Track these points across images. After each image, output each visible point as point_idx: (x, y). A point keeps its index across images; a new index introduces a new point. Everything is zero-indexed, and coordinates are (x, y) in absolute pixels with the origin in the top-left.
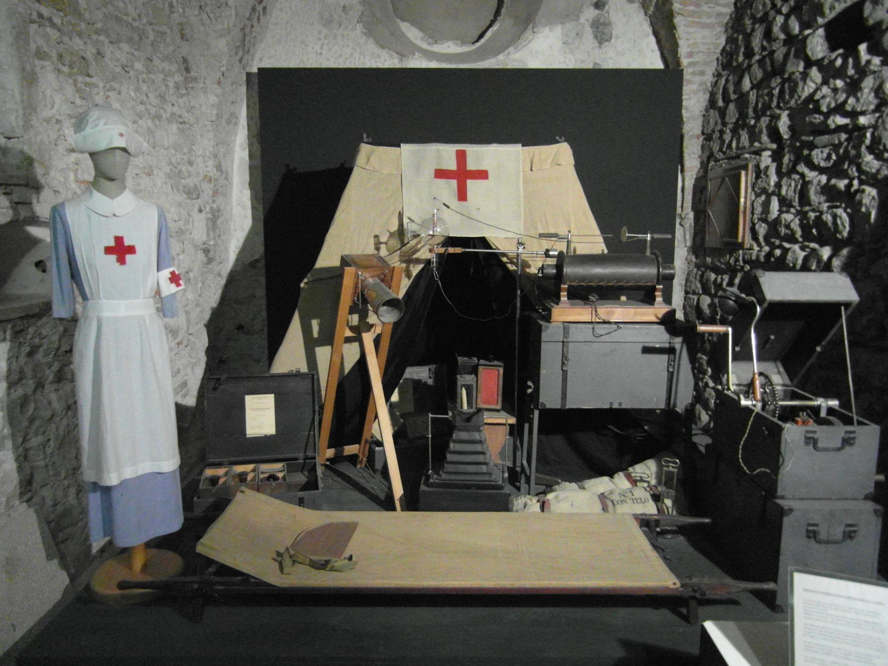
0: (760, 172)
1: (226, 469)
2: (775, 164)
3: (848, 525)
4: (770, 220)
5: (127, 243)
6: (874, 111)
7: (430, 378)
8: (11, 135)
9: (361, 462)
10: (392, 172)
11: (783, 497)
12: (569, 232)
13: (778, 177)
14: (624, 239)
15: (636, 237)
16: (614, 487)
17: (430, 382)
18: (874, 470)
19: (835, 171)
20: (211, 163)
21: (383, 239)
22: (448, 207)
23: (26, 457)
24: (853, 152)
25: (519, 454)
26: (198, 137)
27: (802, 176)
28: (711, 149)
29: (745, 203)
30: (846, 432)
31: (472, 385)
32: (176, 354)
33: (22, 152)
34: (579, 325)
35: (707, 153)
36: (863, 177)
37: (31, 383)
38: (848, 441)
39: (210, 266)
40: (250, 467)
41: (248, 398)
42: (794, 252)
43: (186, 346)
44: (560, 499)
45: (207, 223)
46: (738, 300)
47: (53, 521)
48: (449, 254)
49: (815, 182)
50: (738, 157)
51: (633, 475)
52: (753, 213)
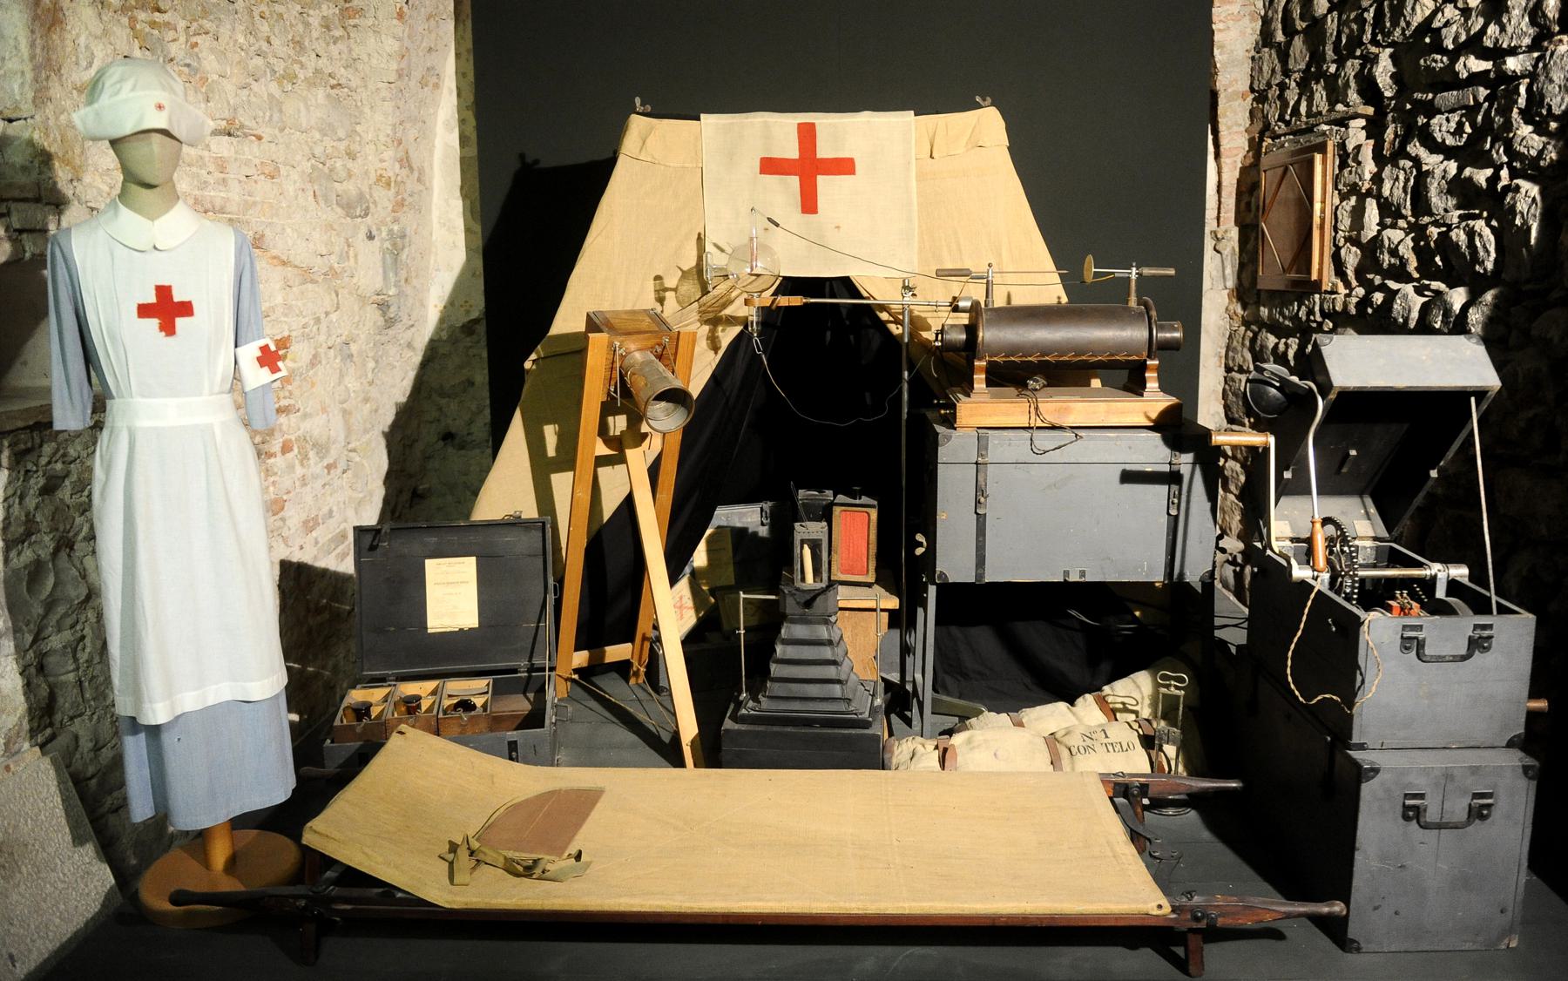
0: (1348, 155)
1: (386, 690)
2: (1372, 142)
3: (1476, 796)
4: (1364, 241)
5: (178, 297)
6: (1530, 49)
7: (763, 524)
8: (13, 116)
9: (637, 674)
10: (687, 165)
11: (1362, 747)
12: (990, 265)
13: (1376, 166)
14: (1089, 278)
15: (1113, 273)
16: (1076, 722)
17: (763, 532)
18: (1526, 693)
19: (1470, 154)
20: (389, 154)
21: (671, 282)
22: (777, 225)
23: (41, 668)
24: (1498, 120)
25: (909, 660)
26: (367, 110)
27: (1417, 162)
28: (1265, 117)
29: (1323, 211)
30: (1476, 627)
31: (821, 540)
32: (324, 485)
33: (30, 143)
34: (1005, 433)
35: (1259, 125)
36: (1517, 165)
37: (47, 542)
38: (1478, 644)
40: (431, 685)
41: (431, 565)
42: (1405, 296)
43: (344, 472)
44: (976, 744)
45: (384, 259)
46: (1284, 386)
48: (779, 308)
49: (1438, 173)
50: (1310, 130)
51: (1110, 699)
52: (1336, 229)
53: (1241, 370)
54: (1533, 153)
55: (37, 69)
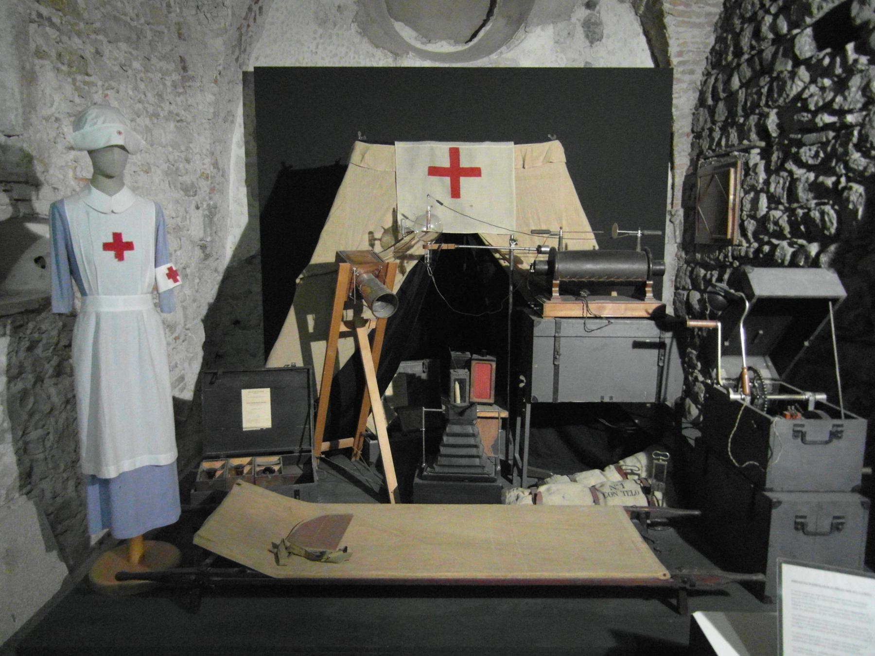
0: (749, 169)
2: (763, 162)
3: (835, 518)
4: (759, 216)
5: (125, 239)
6: (861, 110)
7: (424, 372)
8: (11, 133)
9: (356, 455)
10: (387, 170)
11: (771, 490)
12: (561, 228)
13: (766, 175)
14: (615, 236)
15: (627, 233)
16: (605, 480)
17: (424, 376)
18: (861, 463)
19: (823, 168)
20: (207, 161)
21: (378, 235)
22: (442, 204)
23: (25, 450)
24: (840, 150)
25: (511, 447)
26: (195, 135)
27: (791, 173)
28: (700, 147)
29: (734, 200)
30: (834, 426)
31: (465, 379)
32: (173, 349)
33: (21, 150)
34: (570, 320)
35: (697, 151)
36: (851, 175)
37: (30, 378)
38: (835, 435)
40: (246, 460)
41: (244, 392)
42: (783, 248)
43: (183, 341)
44: (552, 491)
45: (204, 220)
46: (727, 295)
48: (443, 251)
49: (803, 179)
50: (727, 154)
51: (624, 468)
52: (742, 210)
53: (684, 289)
54: (861, 168)
55: (24, 107)
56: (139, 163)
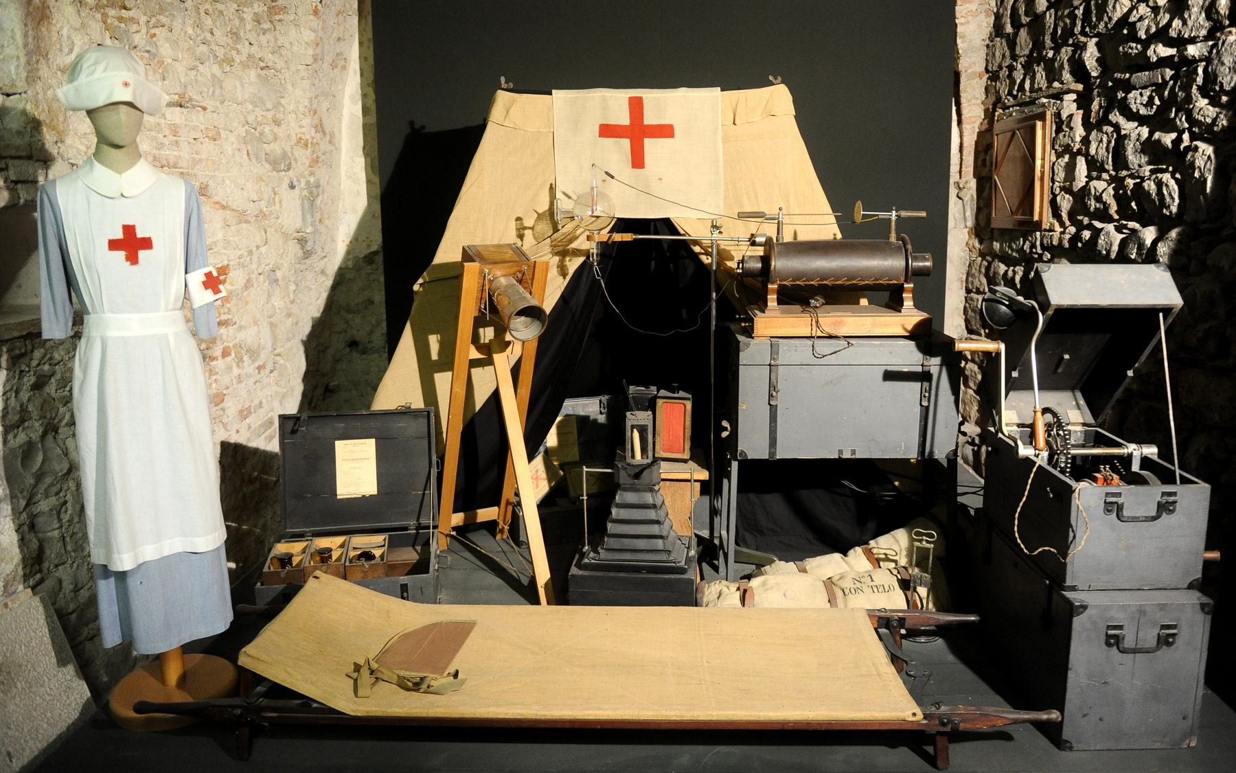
0: (1063, 122)
2: (1081, 112)
3: (1164, 627)
4: (1075, 190)
5: (140, 234)
6: (1206, 39)
7: (601, 413)
8: (11, 91)
9: (502, 531)
10: (541, 130)
11: (1073, 588)
12: (780, 209)
13: (1085, 130)
14: (858, 219)
15: (878, 215)
16: (848, 569)
17: (602, 419)
18: (1203, 546)
19: (1159, 121)
20: (306, 121)
21: (529, 222)
22: (613, 177)
23: (32, 527)
24: (1181, 94)
25: (717, 520)
26: (289, 86)
27: (1117, 127)
28: (997, 92)
29: (1043, 166)
30: (1164, 494)
31: (647, 425)
32: (255, 383)
33: (24, 112)
34: (792, 341)
35: (992, 99)
36: (1196, 130)
37: (37, 427)
38: (1165, 508)
39: (308, 261)
40: (339, 540)
41: (340, 445)
42: (1108, 234)
43: (271, 372)
44: (769, 586)
45: (303, 204)
46: (1012, 304)
47: (73, 612)
48: (614, 243)
49: (1134, 136)
50: (1032, 102)
51: (875, 551)
52: (1053, 181)
54: (1209, 120)
55: (29, 54)
56: (203, 127)
